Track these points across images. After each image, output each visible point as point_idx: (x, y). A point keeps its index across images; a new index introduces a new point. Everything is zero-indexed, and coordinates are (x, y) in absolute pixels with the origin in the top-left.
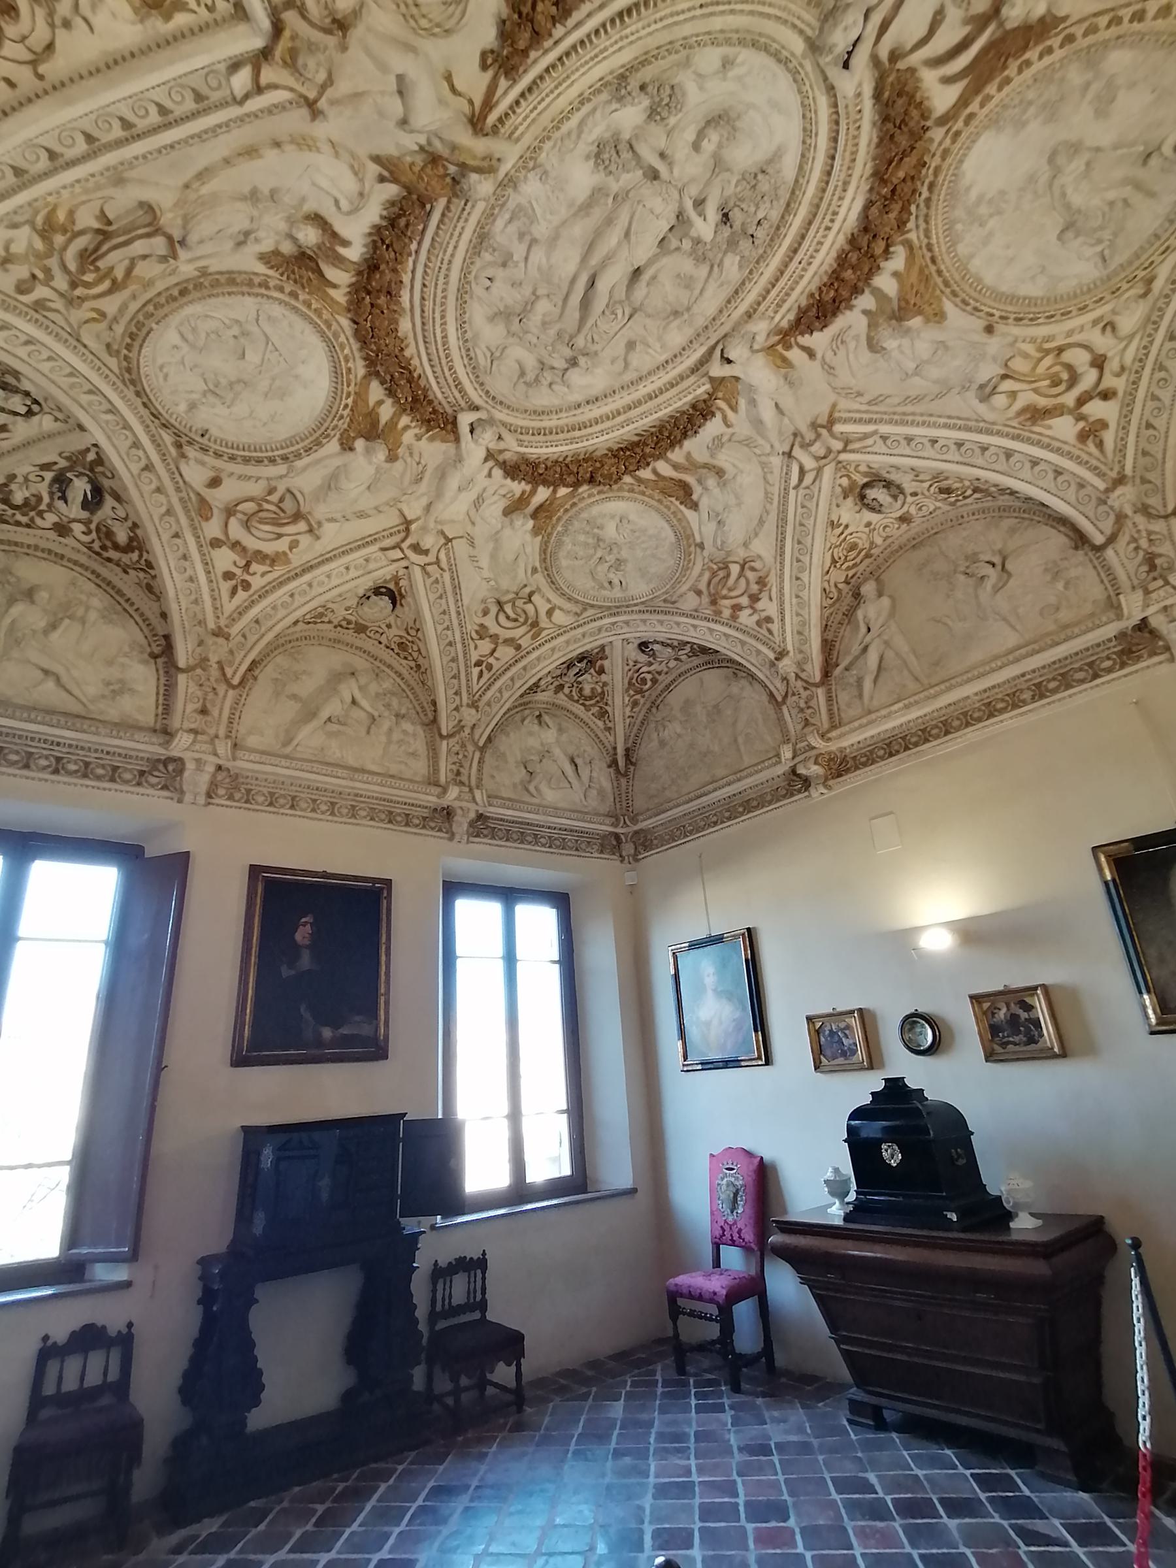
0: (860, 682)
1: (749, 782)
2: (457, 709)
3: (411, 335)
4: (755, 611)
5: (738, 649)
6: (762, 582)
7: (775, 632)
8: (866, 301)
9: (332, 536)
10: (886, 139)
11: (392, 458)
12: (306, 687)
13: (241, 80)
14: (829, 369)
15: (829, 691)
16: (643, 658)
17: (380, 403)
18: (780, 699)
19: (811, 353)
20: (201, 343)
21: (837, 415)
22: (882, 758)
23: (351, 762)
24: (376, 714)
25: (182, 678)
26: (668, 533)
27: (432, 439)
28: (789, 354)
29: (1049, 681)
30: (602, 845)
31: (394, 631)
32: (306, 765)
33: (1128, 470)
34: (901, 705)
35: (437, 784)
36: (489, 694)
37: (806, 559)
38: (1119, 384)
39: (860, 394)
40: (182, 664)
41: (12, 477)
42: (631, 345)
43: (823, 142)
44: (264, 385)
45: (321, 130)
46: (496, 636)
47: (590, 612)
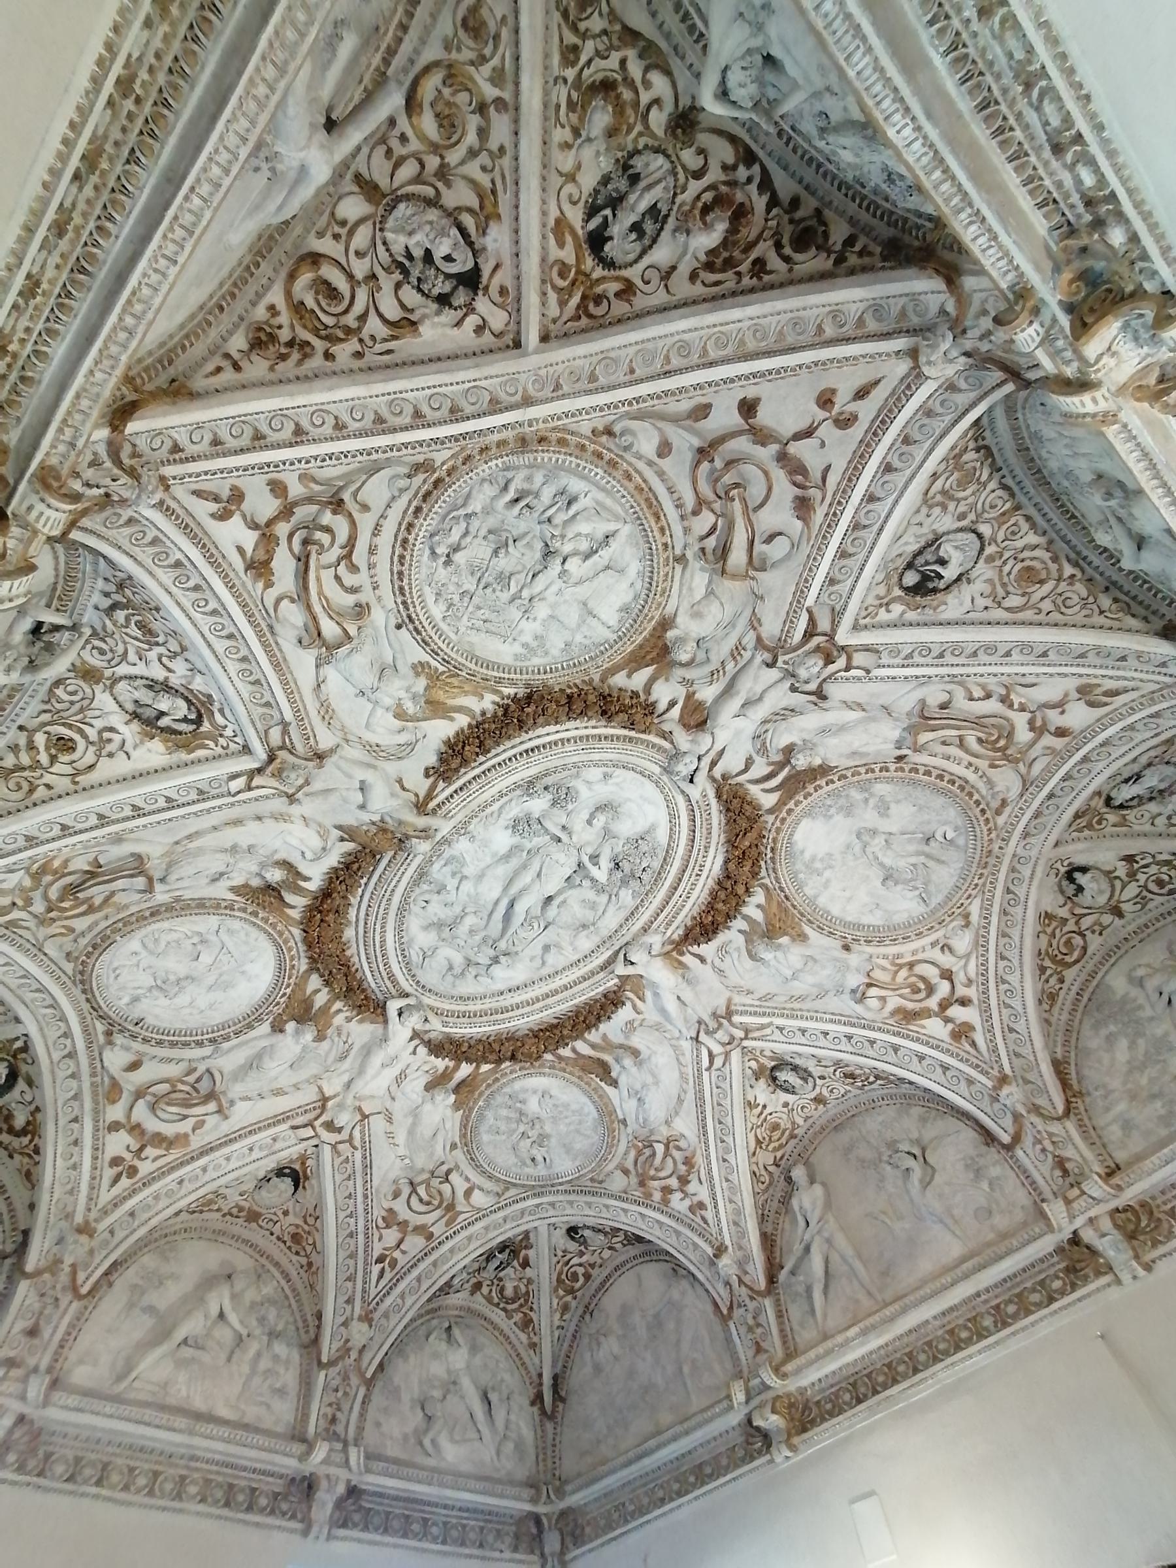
0: (809, 1290)
1: (698, 1436)
2: (345, 1324)
4: (686, 1195)
5: (673, 1240)
6: (688, 1162)
8: (739, 924)
9: (243, 1114)
10: (731, 822)
11: (320, 1037)
12: (167, 1296)
13: (240, 782)
15: (777, 1303)
16: (573, 1246)
23: (199, 1404)
24: (244, 1332)
25: (23, 1286)
26: (590, 1109)
27: (361, 1021)
30: (517, 1536)
31: (291, 1219)
32: (135, 1412)
33: (1007, 1070)
35: (303, 1440)
36: (389, 1301)
37: (729, 1140)
38: (972, 993)
39: (749, 992)
40: (29, 1267)
42: (547, 948)
44: (211, 979)
45: (295, 810)
46: (406, 1222)
47: (512, 1192)
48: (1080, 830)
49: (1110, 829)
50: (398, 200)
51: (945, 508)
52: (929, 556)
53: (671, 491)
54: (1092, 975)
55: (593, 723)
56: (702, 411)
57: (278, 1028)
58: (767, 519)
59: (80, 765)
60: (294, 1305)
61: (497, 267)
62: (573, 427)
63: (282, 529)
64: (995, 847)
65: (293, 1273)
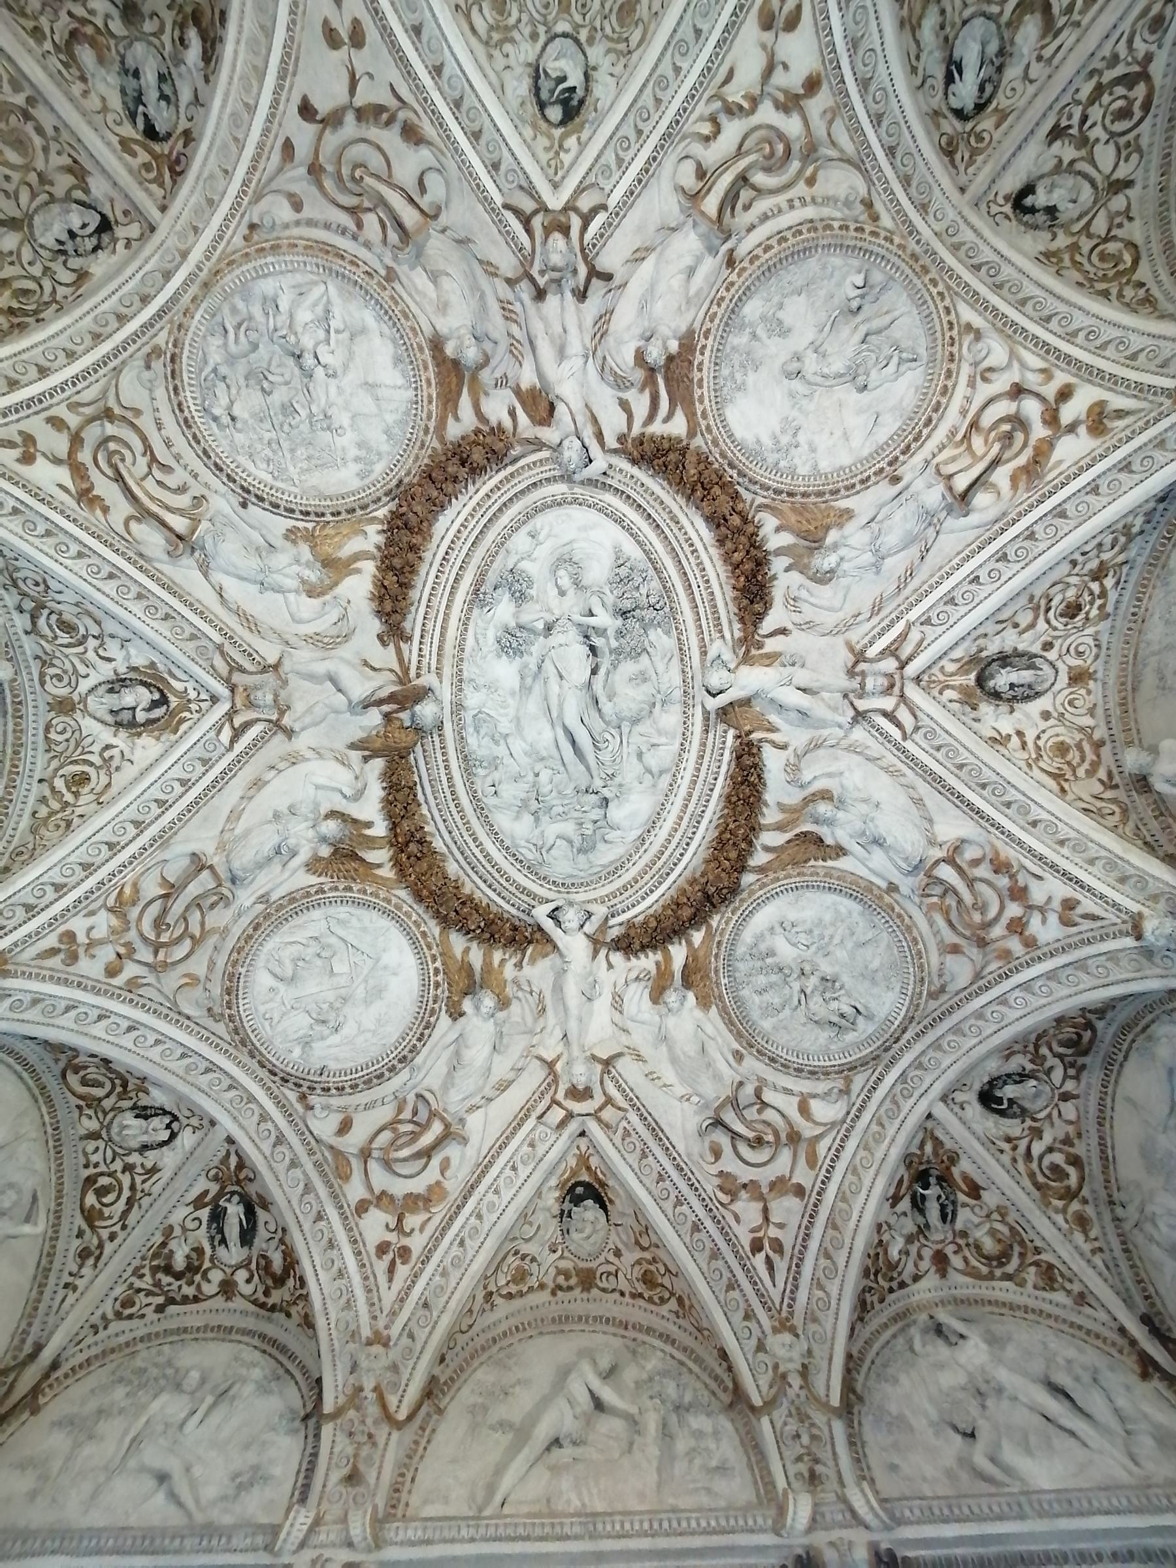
2: (761, 1347)
4: (1042, 910)
5: (1087, 981)
6: (1000, 866)
7: (1098, 911)
8: (778, 565)
11: (504, 1003)
14: (808, 626)
16: (1013, 1127)
17: (467, 950)
19: (783, 631)
20: (289, 972)
21: (858, 647)
25: (327, 1430)
26: (846, 905)
27: (533, 961)
28: (767, 649)
36: (802, 1296)
37: (1012, 795)
38: (1062, 378)
41: (168, 1232)
44: (360, 992)
45: (301, 743)
47: (859, 1081)
48: (971, 162)
50: (31, 218)
51: (512, 41)
52: (545, 85)
53: (327, 226)
56: (288, 147)
57: (456, 1014)
58: (405, 174)
59: (98, 789)
60: (695, 1368)
61: (112, 201)
62: (230, 249)
63: (85, 456)
64: (912, 245)
65: (672, 1329)
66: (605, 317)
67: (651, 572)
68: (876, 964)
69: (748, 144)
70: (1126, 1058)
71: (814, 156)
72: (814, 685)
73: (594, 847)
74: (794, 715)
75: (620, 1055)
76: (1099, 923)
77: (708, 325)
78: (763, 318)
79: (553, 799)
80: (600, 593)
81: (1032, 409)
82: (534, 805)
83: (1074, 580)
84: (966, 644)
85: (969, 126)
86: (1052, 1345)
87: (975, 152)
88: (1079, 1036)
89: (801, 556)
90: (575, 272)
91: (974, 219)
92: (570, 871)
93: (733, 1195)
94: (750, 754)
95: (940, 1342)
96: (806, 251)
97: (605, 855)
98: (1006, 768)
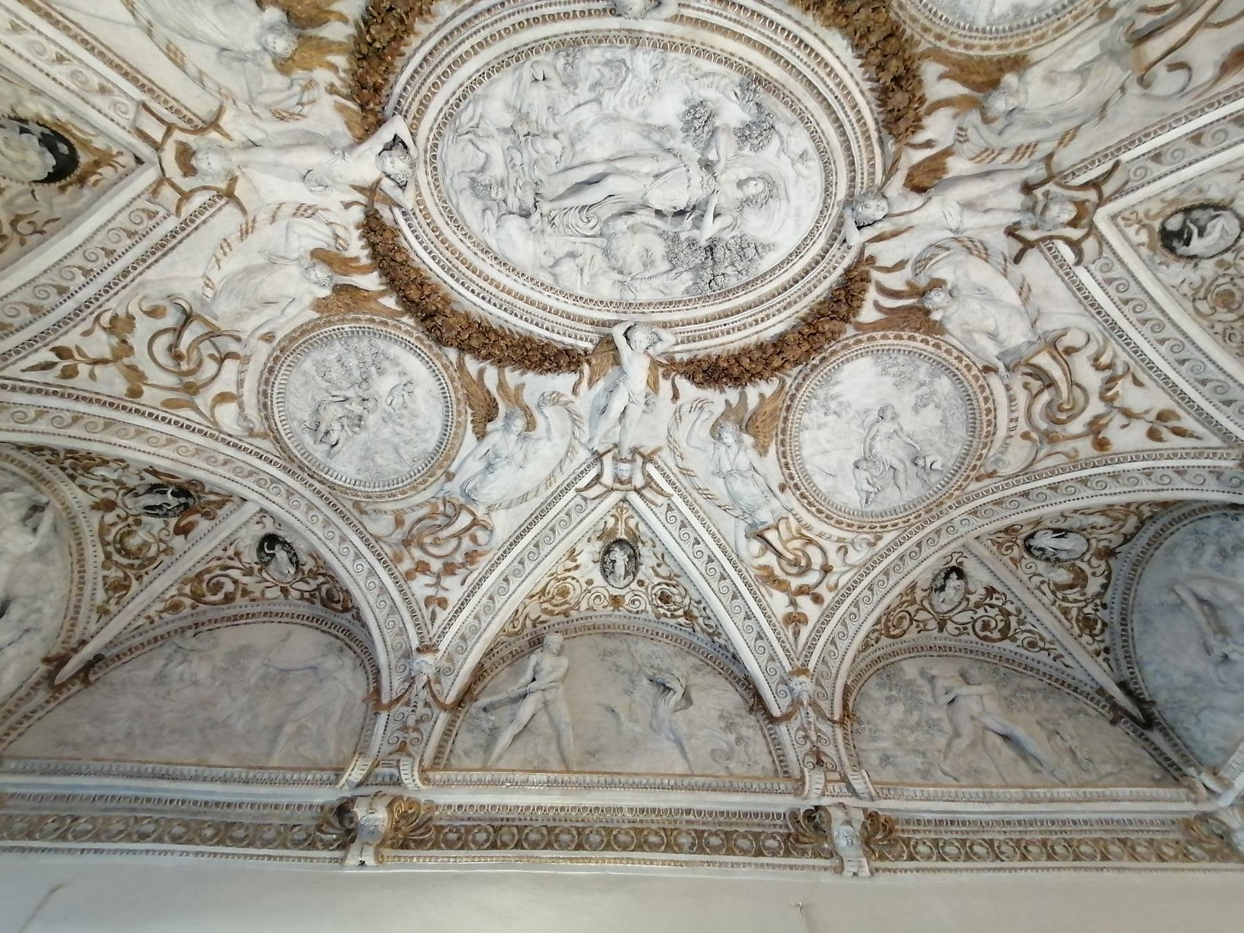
3: (440, 20)
4: (437, 584)
5: (381, 615)
6: (471, 557)
7: (438, 621)
8: (732, 395)
14: (678, 417)
15: (451, 723)
16: (250, 557)
18: (385, 700)
19: (676, 396)
21: (656, 457)
22: (479, 846)
26: (432, 439)
27: (341, 109)
29: (711, 834)
33: (811, 666)
34: (543, 777)
36: (20, 398)
37: (529, 565)
38: (828, 597)
43: (801, 264)
47: (266, 445)
49: (1006, 559)
54: (894, 654)
55: (867, 86)
66: (979, 250)
67: (745, 279)
68: (379, 460)
69: (1076, 390)
70: (323, 631)
71: (1046, 440)
72: (627, 420)
73: (477, 196)
74: (603, 402)
75: (244, 211)
76: (428, 622)
77: (944, 348)
78: (933, 393)
79: (528, 154)
80: (733, 226)
81: (812, 578)
82: (522, 129)
83: (687, 601)
84: (649, 534)
85: (1019, 542)
86: (52, 596)
87: (1000, 545)
88: (338, 602)
89: (737, 414)
90: (1035, 228)
91: (954, 545)
92: (451, 165)
93: (111, 329)
94: (570, 363)
95: (24, 511)
96: (973, 428)
97: (469, 209)
98: (552, 560)
